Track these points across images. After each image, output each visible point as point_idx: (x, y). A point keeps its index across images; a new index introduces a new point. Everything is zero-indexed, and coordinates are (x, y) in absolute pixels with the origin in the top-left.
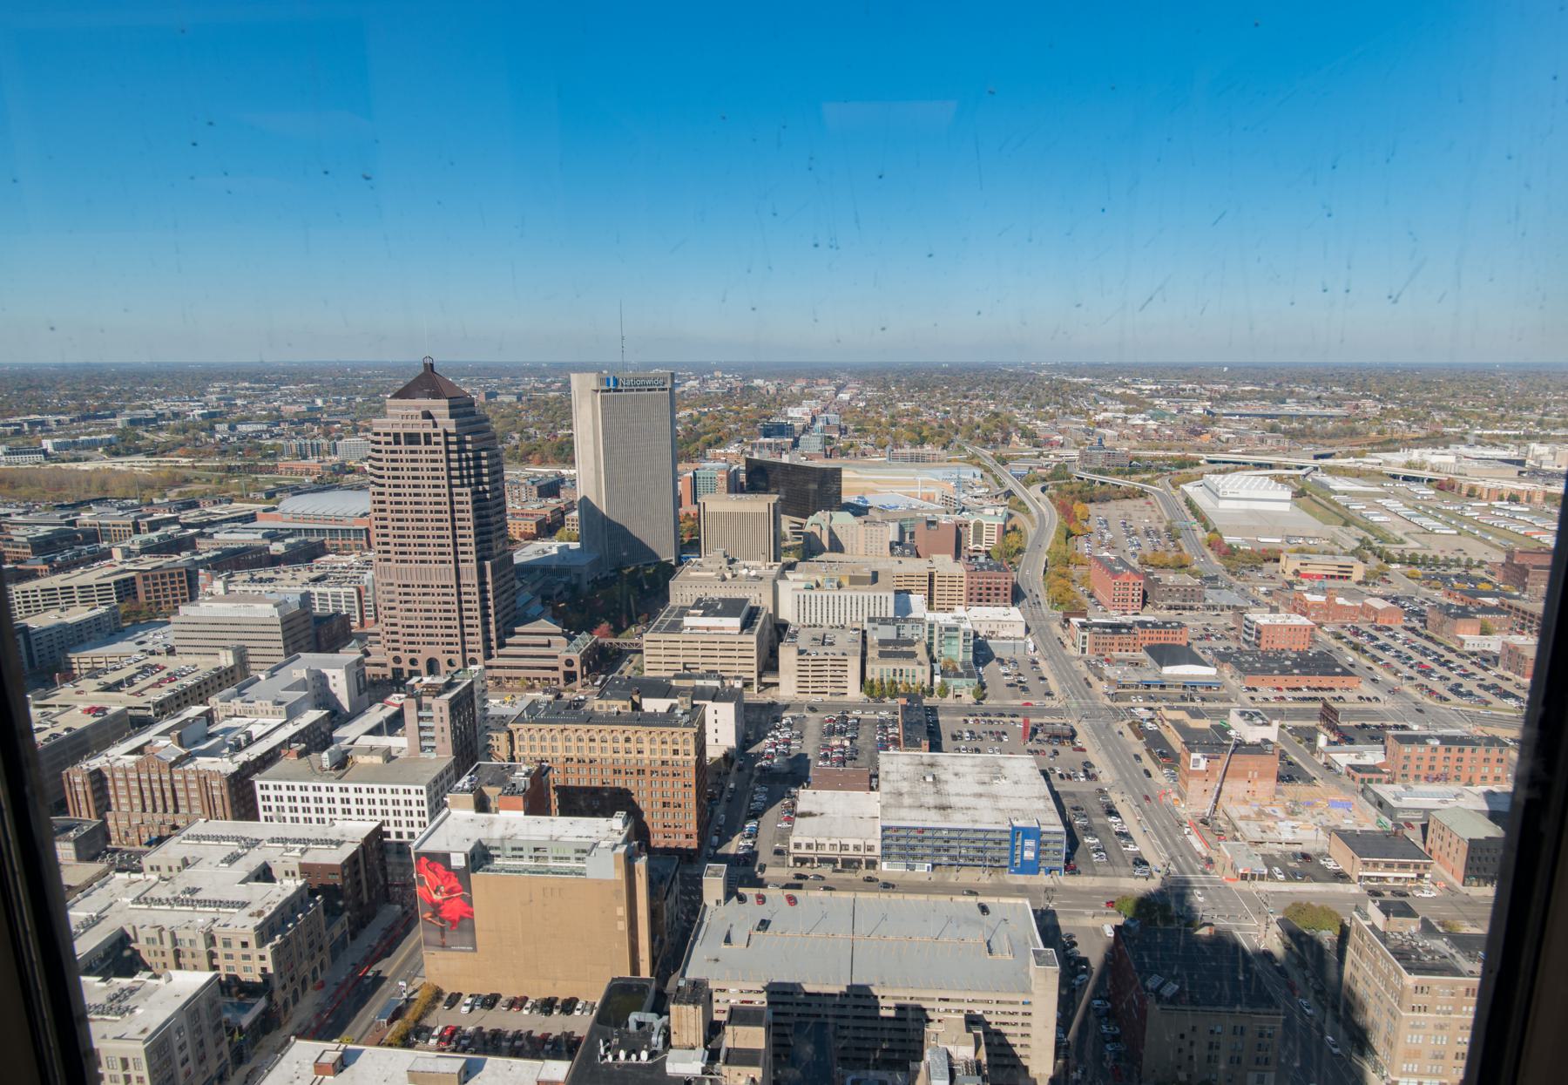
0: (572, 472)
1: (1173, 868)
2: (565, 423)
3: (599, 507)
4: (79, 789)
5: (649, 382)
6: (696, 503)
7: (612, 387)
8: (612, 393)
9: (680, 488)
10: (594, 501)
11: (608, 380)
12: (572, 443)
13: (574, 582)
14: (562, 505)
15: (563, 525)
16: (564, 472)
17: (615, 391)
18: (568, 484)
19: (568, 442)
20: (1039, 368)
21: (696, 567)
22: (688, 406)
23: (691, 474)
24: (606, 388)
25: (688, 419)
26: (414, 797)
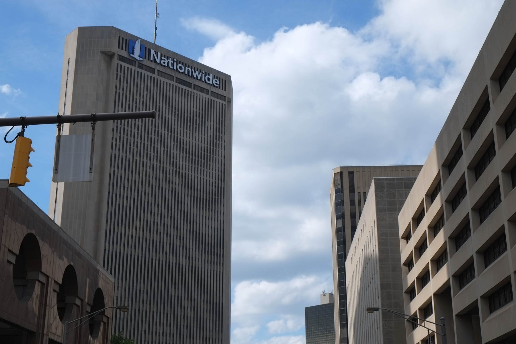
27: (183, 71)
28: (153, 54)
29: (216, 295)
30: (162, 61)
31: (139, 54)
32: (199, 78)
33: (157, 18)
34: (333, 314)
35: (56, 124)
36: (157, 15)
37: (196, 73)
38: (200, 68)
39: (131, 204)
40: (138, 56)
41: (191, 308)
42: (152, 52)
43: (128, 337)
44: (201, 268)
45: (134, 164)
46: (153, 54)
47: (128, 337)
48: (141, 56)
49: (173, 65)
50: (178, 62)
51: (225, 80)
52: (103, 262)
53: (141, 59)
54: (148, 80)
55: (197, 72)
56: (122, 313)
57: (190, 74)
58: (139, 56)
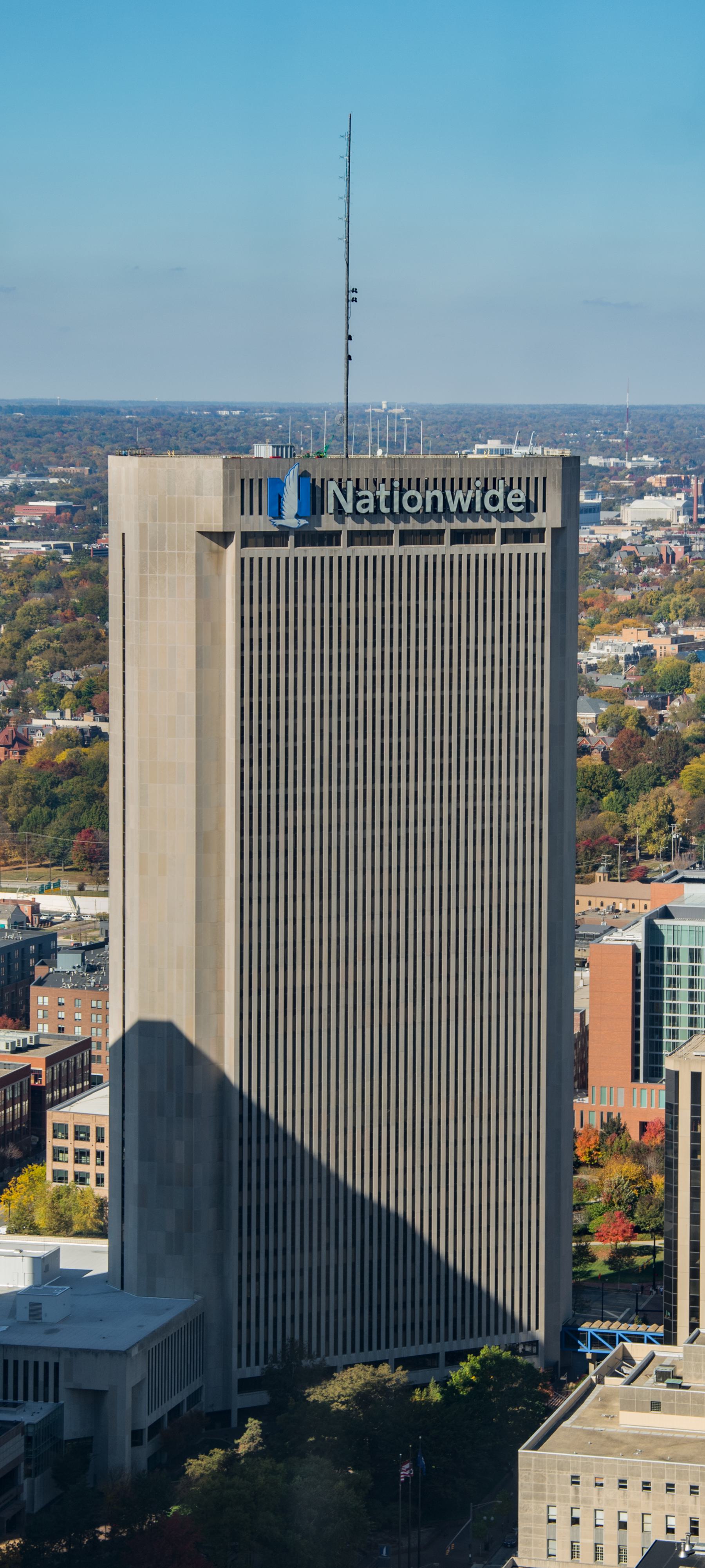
0: (90, 906)
1: (628, 476)
2: (64, 679)
3: (209, 1050)
4: (518, 452)
5: (461, 498)
6: (654, 1072)
7: (290, 521)
8: (289, 551)
9: (581, 1000)
10: (189, 1030)
11: (278, 485)
12: (102, 770)
13: (71, 1429)
14: (36, 1060)
15: (36, 1154)
16: (50, 903)
17: (305, 537)
18: (67, 962)
19: (73, 769)
20: (366, 406)
21: (647, 1384)
22: (627, 613)
23: (637, 935)
24: (261, 523)
25: (630, 676)
26: (91, 1168)
27: (418, 507)
28: (335, 494)
29: (371, 1262)
30: (359, 504)
31: (295, 510)
32: (465, 509)
33: (351, 304)
36: (351, 296)
41: (249, 1254)
42: (333, 487)
43: (297, 1337)
44: (345, 1266)
46: (335, 494)
47: (297, 1337)
50: (405, 485)
52: (237, 1199)
53: (303, 522)
55: (459, 495)
56: (645, 1106)
58: (297, 516)
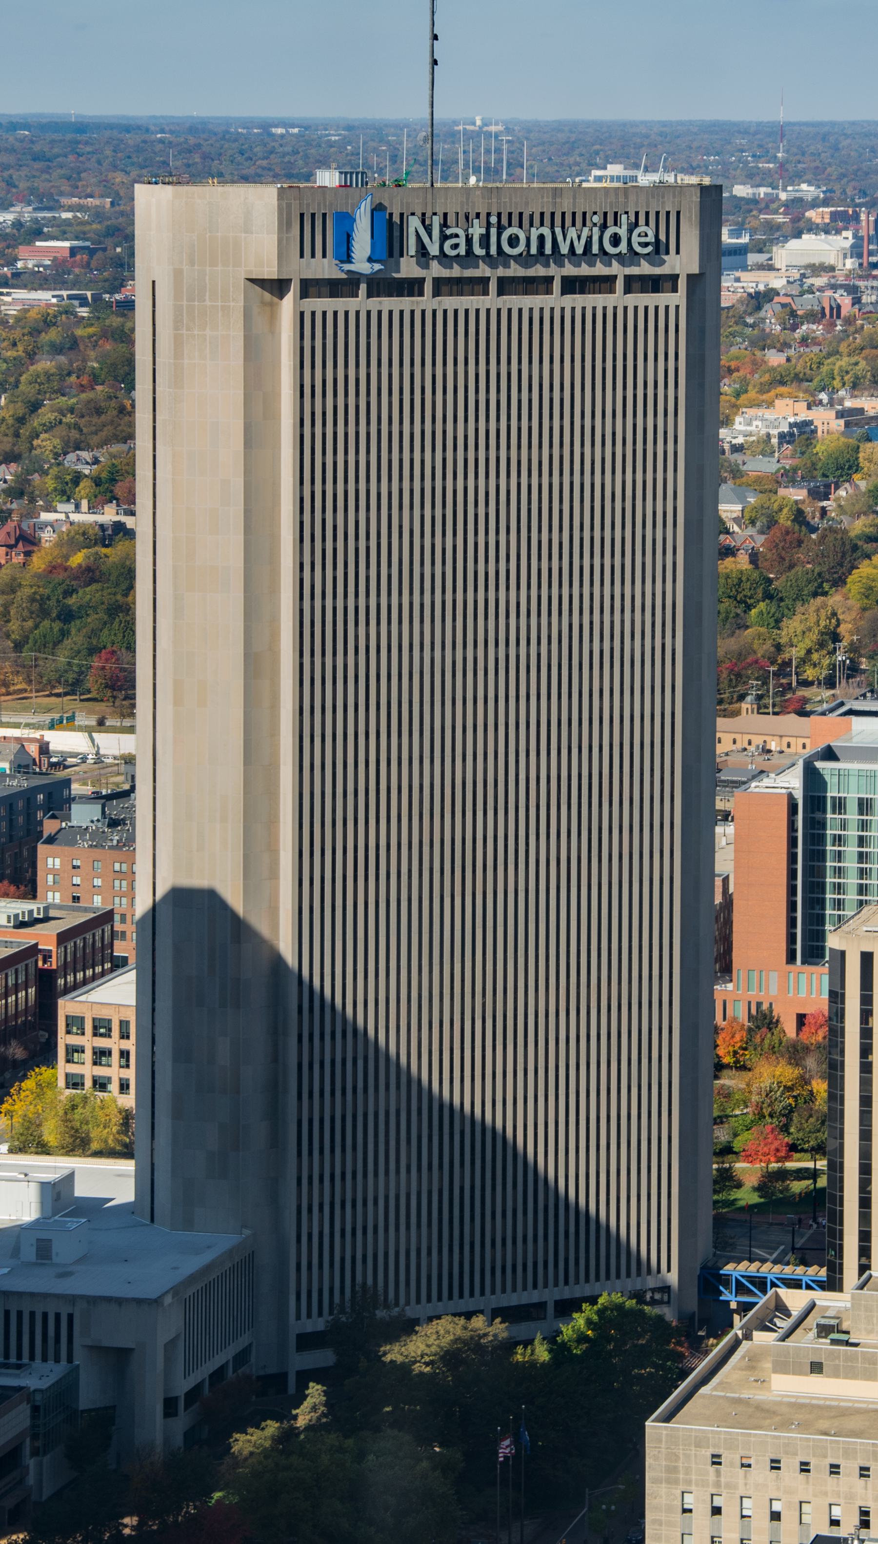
28: (417, 231)
30: (447, 244)
31: (368, 252)
32: (579, 250)
34: (687, 355)
35: (134, 1106)
37: (568, 242)
38: (707, 1197)
39: (355, 1246)
40: (366, 259)
42: (414, 223)
43: (370, 1281)
45: (360, 1063)
46: (417, 231)
47: (370, 1281)
48: (374, 258)
49: (485, 240)
51: (678, 213)
54: (387, 1198)
55: (572, 233)
57: (548, 250)
58: (370, 260)
